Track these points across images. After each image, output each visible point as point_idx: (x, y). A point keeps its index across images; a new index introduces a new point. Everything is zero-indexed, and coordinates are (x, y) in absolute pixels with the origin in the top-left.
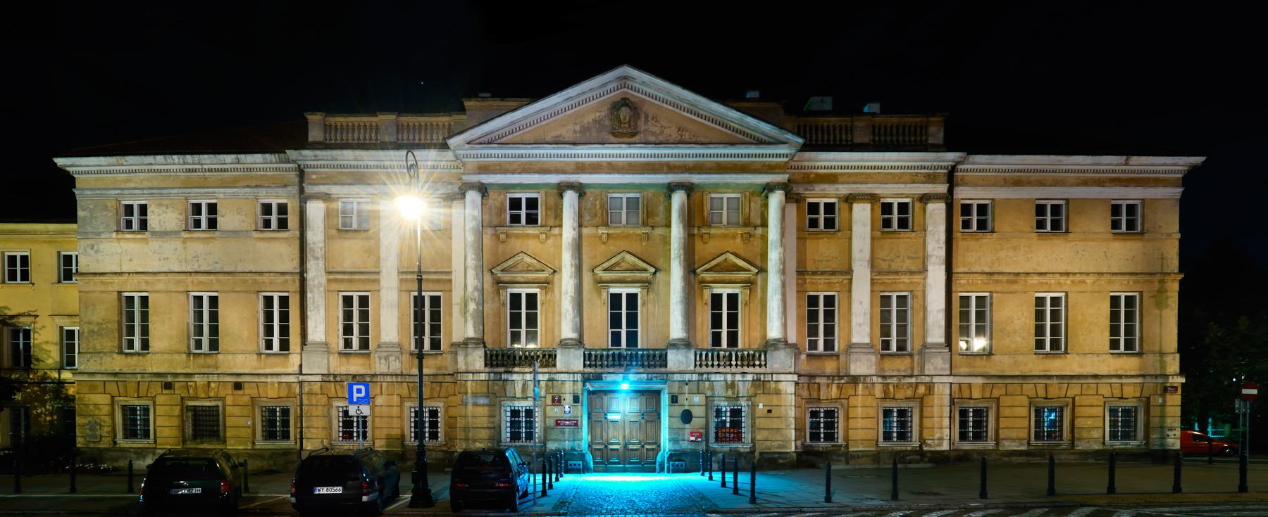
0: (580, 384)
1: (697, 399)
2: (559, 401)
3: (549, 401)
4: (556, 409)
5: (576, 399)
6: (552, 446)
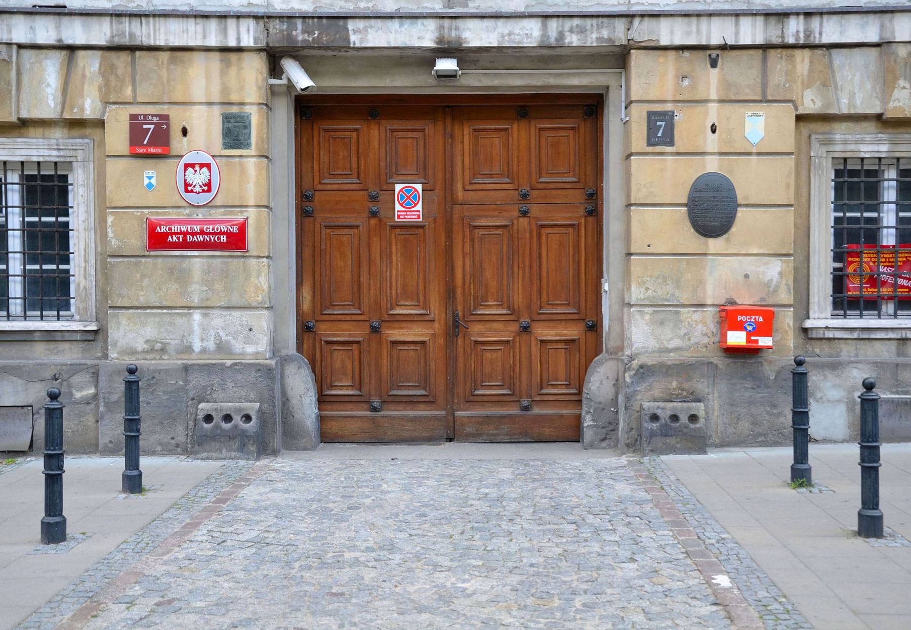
0: (254, 69)
1: (757, 126)
2: (162, 136)
3: (117, 137)
4: (150, 174)
5: (235, 133)
6: (130, 337)
